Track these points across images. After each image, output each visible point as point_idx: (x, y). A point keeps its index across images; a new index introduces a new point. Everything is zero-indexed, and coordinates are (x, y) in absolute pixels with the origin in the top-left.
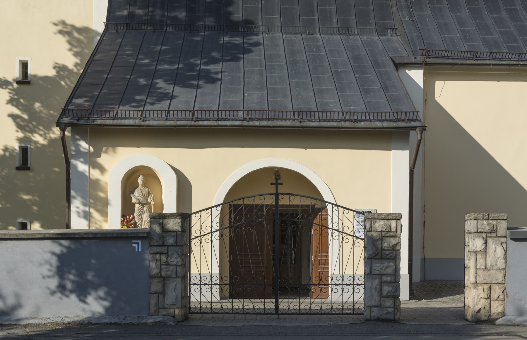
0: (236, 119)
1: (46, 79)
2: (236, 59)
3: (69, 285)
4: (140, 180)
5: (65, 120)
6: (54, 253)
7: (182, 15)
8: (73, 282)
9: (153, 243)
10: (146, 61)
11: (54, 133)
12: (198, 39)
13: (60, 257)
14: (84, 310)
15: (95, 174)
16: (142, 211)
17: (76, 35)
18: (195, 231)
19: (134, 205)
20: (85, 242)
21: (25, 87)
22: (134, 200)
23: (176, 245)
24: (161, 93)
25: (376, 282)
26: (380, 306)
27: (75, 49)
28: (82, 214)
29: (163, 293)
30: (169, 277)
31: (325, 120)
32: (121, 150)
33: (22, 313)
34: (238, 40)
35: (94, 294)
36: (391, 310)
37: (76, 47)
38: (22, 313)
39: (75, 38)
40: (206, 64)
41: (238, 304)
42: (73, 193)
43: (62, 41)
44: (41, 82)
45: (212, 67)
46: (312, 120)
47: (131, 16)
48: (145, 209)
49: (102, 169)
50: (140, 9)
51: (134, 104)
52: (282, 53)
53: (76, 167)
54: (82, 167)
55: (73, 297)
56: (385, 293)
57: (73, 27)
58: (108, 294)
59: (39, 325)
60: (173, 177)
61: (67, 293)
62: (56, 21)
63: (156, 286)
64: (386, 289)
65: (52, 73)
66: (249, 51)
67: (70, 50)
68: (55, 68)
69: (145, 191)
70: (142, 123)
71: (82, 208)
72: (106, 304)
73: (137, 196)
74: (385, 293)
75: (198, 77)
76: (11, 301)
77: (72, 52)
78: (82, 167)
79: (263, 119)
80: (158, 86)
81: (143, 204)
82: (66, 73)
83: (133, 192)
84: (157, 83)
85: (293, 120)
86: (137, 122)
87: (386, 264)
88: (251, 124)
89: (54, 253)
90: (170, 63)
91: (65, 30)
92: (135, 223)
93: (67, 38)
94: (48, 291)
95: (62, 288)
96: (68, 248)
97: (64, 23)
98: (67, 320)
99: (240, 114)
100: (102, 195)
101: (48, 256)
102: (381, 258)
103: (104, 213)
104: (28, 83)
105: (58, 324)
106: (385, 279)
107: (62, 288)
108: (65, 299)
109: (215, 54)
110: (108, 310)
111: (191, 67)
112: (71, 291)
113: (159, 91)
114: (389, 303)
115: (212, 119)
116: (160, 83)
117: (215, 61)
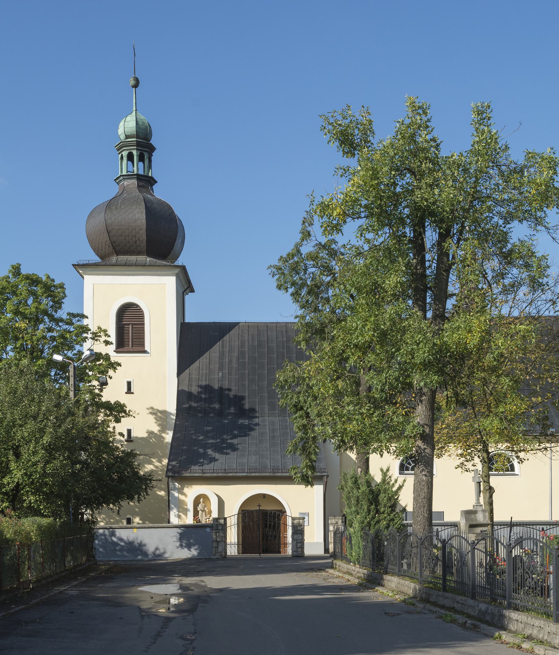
0: (244, 472)
1: (142, 439)
2: (246, 435)
3: (184, 545)
4: (201, 500)
5: (170, 474)
6: (178, 533)
7: (217, 406)
8: (185, 543)
9: (214, 529)
10: (201, 438)
11: (147, 468)
12: (226, 421)
13: (180, 534)
14: (190, 554)
15: (182, 497)
16: (202, 514)
17: (159, 414)
18: (228, 525)
19: (199, 511)
20: (190, 529)
21: (130, 443)
22: (199, 509)
23: (222, 530)
24: (211, 458)
25: (295, 542)
26: (296, 551)
27: (159, 422)
28: (177, 516)
29: (218, 547)
30: (220, 541)
31: (284, 473)
32: (194, 487)
33: (166, 555)
34: (246, 422)
35: (193, 548)
36: (300, 552)
37: (159, 421)
38: (166, 555)
39: (158, 416)
40: (231, 439)
41: (246, 555)
42: (172, 506)
43: (152, 417)
44: (139, 440)
45: (235, 441)
46: (278, 473)
47: (190, 407)
48: (204, 513)
49: (185, 495)
50: (195, 403)
51: (199, 464)
52: (268, 431)
53: (173, 495)
54: (176, 494)
55: (186, 549)
56: (298, 546)
57: (158, 410)
58: (198, 547)
59: (172, 560)
60: (217, 499)
61: (184, 547)
62: (148, 408)
63: (215, 545)
64: (299, 545)
65: (145, 435)
66: (253, 430)
67: (156, 423)
68: (147, 432)
69: (203, 505)
70: (203, 475)
71: (177, 513)
72: (198, 551)
73: (200, 507)
74: (298, 546)
75: (227, 448)
76: (162, 551)
77: (157, 424)
78: (176, 494)
79: (256, 472)
80: (209, 453)
81: (203, 511)
82: (154, 435)
83: (198, 506)
84: (208, 452)
85: (190, 642)
86: (200, 475)
87: (299, 536)
88: (251, 475)
89: (178, 533)
90: (213, 438)
91: (153, 412)
92: (199, 520)
93: (154, 416)
94: (176, 547)
95: (181, 546)
96: (183, 530)
97: (152, 408)
98: (182, 558)
99: (246, 470)
100: (186, 507)
101: (176, 534)
102: (297, 534)
103: (186, 515)
104: (132, 441)
105: (179, 559)
106: (298, 541)
107: (181, 546)
108: (182, 550)
109: (236, 432)
110: (198, 553)
111: (223, 441)
112: (185, 547)
113: (210, 456)
114: (300, 550)
115: (233, 473)
116: (210, 452)
117: (235, 437)
